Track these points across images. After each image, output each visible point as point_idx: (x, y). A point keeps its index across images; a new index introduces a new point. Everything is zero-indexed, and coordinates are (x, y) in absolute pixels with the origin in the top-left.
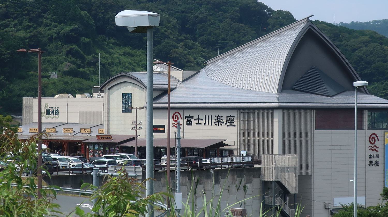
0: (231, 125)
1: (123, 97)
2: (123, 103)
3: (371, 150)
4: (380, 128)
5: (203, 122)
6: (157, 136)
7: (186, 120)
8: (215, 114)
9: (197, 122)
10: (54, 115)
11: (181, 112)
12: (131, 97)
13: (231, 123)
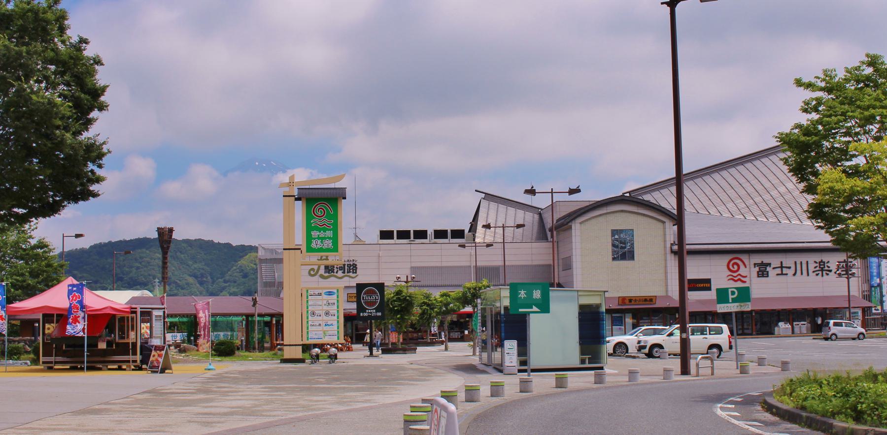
1: (613, 235)
2: (613, 245)
5: (791, 272)
6: (693, 296)
7: (757, 269)
9: (778, 271)
10: (344, 272)
11: (745, 258)
12: (621, 231)
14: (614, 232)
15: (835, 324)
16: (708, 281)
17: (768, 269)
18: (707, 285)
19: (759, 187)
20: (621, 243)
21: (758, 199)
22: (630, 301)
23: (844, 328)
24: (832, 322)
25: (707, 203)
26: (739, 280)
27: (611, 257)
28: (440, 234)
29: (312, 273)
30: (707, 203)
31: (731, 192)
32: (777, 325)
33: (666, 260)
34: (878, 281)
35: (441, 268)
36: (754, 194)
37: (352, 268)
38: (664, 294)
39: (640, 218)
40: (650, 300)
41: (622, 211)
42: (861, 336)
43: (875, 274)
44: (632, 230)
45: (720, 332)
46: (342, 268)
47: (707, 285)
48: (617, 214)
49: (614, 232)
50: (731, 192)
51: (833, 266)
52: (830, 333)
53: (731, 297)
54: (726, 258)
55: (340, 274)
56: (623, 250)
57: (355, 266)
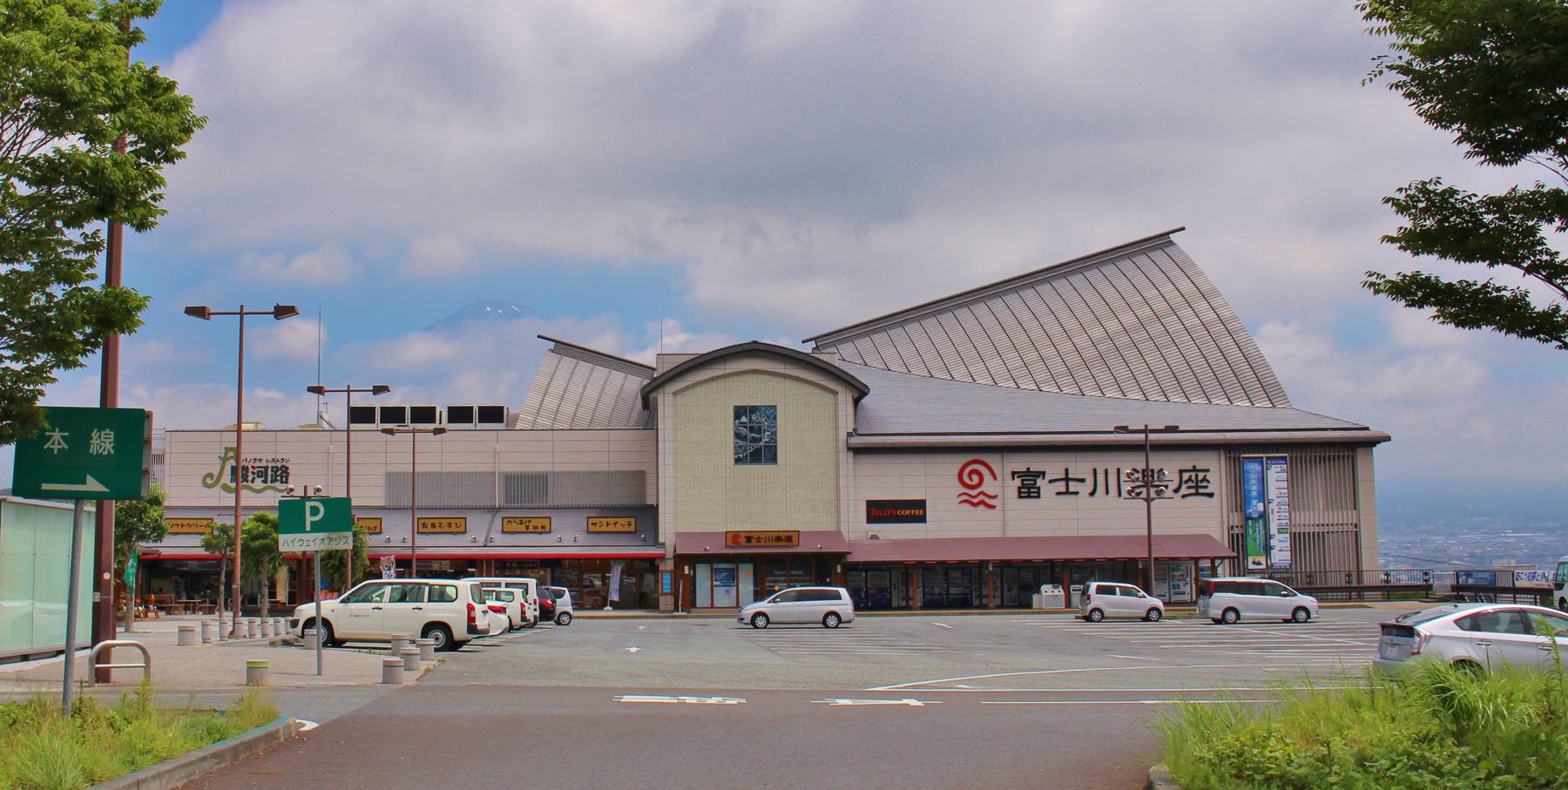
0: (1197, 494)
2: (737, 435)
3: (967, 506)
4: (890, 570)
7: (1018, 482)
8: (1130, 463)
9: (1061, 486)
10: (265, 481)
11: (993, 460)
12: (754, 409)
13: (1197, 487)
14: (739, 412)
15: (1100, 590)
16: (921, 504)
17: (1040, 482)
18: (918, 512)
19: (1053, 328)
20: (752, 429)
21: (1048, 351)
22: (749, 539)
23: (1118, 597)
24: (1094, 585)
25: (950, 358)
26: (982, 502)
27: (731, 457)
28: (460, 415)
29: (209, 481)
30: (950, 358)
31: (1000, 338)
32: (1038, 591)
33: (837, 464)
34: (1260, 507)
35: (441, 474)
36: (1042, 343)
37: (282, 473)
38: (832, 528)
39: (788, 383)
40: (788, 538)
41: (755, 372)
42: (1154, 615)
43: (1254, 494)
44: (774, 407)
45: (838, 597)
46: (263, 473)
47: (918, 512)
48: (747, 378)
49: (739, 412)
50: (1000, 338)
51: (1171, 474)
52: (1089, 607)
53: (309, 519)
54: (959, 461)
55: (259, 484)
56: (756, 441)
57: (285, 470)
